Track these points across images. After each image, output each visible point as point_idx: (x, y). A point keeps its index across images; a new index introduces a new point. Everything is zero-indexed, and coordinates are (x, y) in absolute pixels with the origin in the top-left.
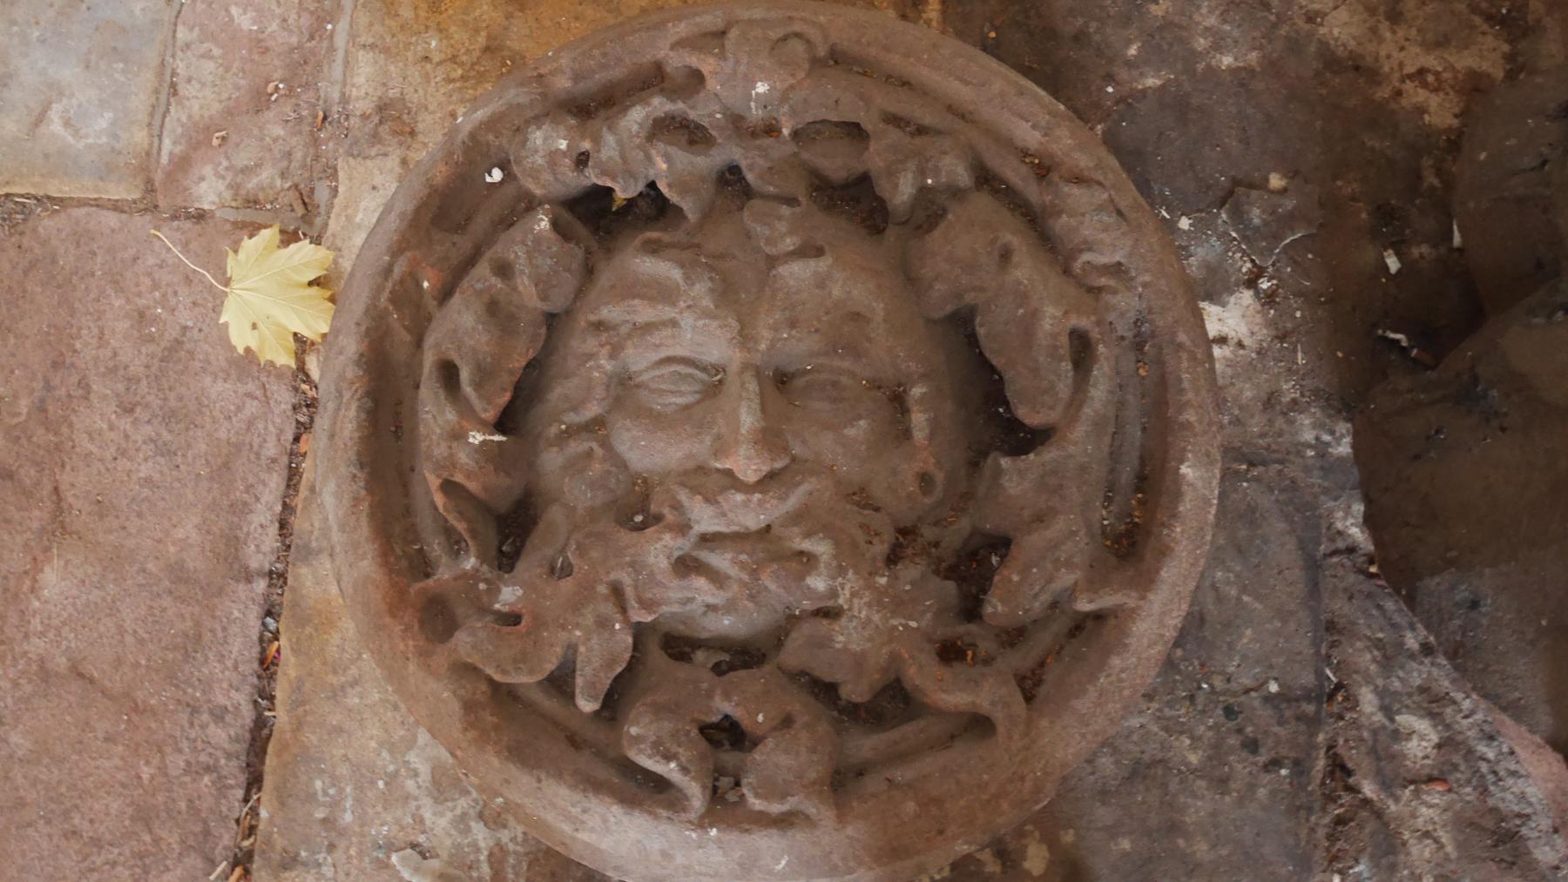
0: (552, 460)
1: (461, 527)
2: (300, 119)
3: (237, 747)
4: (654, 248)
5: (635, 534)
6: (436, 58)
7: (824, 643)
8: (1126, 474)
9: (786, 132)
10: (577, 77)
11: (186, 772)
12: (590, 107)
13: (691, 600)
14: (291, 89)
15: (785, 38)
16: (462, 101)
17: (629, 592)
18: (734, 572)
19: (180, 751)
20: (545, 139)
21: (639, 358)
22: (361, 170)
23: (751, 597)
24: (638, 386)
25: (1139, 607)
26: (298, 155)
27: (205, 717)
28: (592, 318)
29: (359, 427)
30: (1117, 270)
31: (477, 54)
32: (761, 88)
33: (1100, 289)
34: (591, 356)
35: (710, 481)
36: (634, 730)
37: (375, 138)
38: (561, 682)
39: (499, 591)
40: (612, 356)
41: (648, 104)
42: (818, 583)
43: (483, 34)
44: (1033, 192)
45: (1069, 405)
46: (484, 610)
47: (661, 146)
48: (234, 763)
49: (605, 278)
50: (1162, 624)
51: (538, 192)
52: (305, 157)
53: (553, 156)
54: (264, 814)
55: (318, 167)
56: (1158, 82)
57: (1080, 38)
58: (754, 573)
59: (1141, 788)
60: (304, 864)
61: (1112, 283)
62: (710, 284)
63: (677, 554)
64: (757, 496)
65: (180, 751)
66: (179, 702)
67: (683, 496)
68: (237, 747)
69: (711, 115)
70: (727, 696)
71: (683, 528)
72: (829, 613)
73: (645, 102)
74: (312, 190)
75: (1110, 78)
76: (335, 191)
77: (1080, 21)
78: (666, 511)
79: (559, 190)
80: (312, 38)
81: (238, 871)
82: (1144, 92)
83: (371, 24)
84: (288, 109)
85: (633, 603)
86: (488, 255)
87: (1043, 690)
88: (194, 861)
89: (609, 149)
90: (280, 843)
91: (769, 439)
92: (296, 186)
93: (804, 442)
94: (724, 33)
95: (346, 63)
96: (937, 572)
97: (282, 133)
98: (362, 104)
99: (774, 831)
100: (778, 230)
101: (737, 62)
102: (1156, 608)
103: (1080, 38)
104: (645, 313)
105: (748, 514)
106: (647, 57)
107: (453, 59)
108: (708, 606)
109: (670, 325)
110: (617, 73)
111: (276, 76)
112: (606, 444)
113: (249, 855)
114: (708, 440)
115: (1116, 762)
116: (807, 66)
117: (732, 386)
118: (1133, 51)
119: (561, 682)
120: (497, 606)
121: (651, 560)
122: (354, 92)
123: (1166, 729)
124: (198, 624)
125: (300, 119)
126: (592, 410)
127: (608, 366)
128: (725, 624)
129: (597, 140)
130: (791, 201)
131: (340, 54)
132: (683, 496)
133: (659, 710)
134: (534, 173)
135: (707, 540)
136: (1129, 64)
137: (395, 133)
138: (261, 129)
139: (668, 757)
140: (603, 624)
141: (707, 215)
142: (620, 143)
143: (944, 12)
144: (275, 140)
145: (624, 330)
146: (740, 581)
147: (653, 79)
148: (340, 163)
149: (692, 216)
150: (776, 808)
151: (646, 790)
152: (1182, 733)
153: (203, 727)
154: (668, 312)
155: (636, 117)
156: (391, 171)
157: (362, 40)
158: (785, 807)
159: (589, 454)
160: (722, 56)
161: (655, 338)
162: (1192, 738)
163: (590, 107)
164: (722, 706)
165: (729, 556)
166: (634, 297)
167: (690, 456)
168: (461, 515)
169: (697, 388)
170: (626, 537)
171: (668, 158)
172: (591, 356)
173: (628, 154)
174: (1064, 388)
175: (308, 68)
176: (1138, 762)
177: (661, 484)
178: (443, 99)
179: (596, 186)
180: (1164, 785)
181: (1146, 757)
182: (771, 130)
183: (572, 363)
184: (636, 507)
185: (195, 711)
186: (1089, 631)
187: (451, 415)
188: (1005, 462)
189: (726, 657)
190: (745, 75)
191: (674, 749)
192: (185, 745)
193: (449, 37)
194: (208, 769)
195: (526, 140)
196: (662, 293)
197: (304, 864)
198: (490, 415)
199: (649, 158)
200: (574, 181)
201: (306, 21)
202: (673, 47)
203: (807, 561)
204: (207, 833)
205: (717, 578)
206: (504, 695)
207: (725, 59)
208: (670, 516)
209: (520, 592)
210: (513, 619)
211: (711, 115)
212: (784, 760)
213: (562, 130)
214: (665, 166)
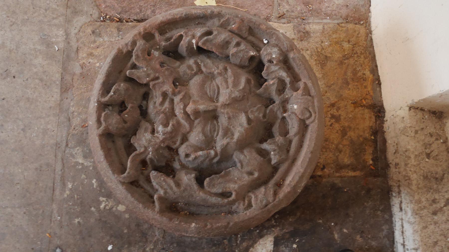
0: (191, 62)
1: (172, 40)
2: (303, 13)
3: (146, 16)
4: (248, 81)
5: (172, 82)
6: (323, 44)
7: (146, 131)
8: (193, 209)
9: (285, 115)
10: (293, 58)
11: (140, 6)
12: (285, 62)
13: (156, 97)
14: (310, 10)
15: (310, 112)
16: (311, 52)
17: (157, 82)
18: (164, 108)
19: (145, 4)
20: (275, 52)
21: (219, 80)
22: (290, 29)
23: (157, 112)
24: (212, 81)
25: (155, 212)
26: (293, 14)
27: (153, 9)
28: (228, 68)
29: (195, 14)
30: (250, 206)
31: (325, 54)
32: (295, 107)
33: (244, 201)
34: (218, 68)
35: (186, 99)
36: (122, 85)
37: (299, 32)
38: (134, 67)
39: (157, 51)
40: (218, 73)
41: (287, 77)
42: (160, 128)
43: (331, 55)
44: (273, 182)
45: (209, 192)
46: (152, 47)
47: (277, 82)
48: (143, 16)
49: (239, 71)
50: (153, 219)
51: (261, 52)
52: (293, 15)
53: (270, 54)
54: (130, 23)
55: (290, 19)
56: (336, 238)
57: (347, 215)
58: (163, 112)
59: (140, 235)
60: (118, 34)
61: (246, 204)
62: (238, 96)
63: (167, 93)
64: (183, 112)
65: (145, 4)
66: (156, 2)
67: (183, 93)
68: (146, 16)
69: (287, 94)
70: (132, 107)
71: (174, 94)
72: (153, 132)
73: (288, 76)
74: (284, 18)
75: (336, 224)
76: (285, 24)
77: (352, 215)
78: (178, 89)
79: (263, 57)
80: (325, 14)
81: (118, 20)
82: (333, 234)
83: (330, 28)
84: (305, 10)
85: (154, 82)
86: (242, 40)
87: (135, 188)
88: (120, 10)
89: (274, 68)
90: (124, 27)
91: (197, 113)
92: (285, 14)
93: (199, 123)
94: (310, 96)
95: (319, 23)
96: (167, 161)
97: (298, 9)
98: (307, 28)
99: (96, 119)
100: (256, 113)
101: (301, 99)
102: (156, 217)
103: (347, 215)
104: (230, 81)
105: (178, 111)
106: (301, 76)
107: (323, 49)
108: (156, 102)
109: (228, 86)
110: (297, 70)
111: (314, 7)
112: (196, 74)
113: (122, 22)
114: (198, 99)
115: (146, 229)
116: (302, 118)
117: (213, 104)
118: (345, 231)
119: (134, 67)
120: (153, 51)
121: (165, 86)
122: (311, 25)
123: (155, 242)
124: (174, 4)
125: (303, 13)
126: (204, 69)
127: (215, 73)
128: (151, 106)
129: (276, 65)
130: (264, 116)
131: (321, 21)
132: (183, 93)
133: (127, 90)
134: (266, 50)
135: (172, 101)
136: (341, 229)
137: (301, 36)
138: (299, 5)
139: (114, 92)
140: (148, 75)
141: (259, 96)
142: (276, 71)
143: (351, 177)
144: (296, 8)
145: (226, 76)
146: (161, 110)
147: (295, 78)
148: (291, 24)
149: (258, 91)
150: (102, 119)
151: (106, 87)
152: (154, 246)
153: (150, 8)
154: (230, 85)
155: (283, 74)
156: (291, 36)
157: (325, 26)
158: (102, 122)
159: (193, 70)
160: (302, 95)
161: (224, 84)
162: (153, 249)
163: (285, 62)
164: (129, 106)
165: (168, 106)
166: (234, 77)
167: (193, 95)
168: (175, 40)
169: (212, 96)
170: (171, 80)
171: (273, 84)
172: (218, 68)
173: (274, 73)
174: (214, 190)
175: (316, 14)
176: (147, 234)
177: (186, 88)
178: (311, 47)
179: (264, 66)
180: (140, 242)
181: (148, 237)
182: (285, 111)
183: (216, 64)
184: (179, 82)
185: (154, 6)
186: (148, 198)
187: (199, 34)
188: (193, 175)
189: (144, 108)
190: (298, 102)
191: (117, 94)
192: (146, 5)
193: (329, 47)
194: (141, 10)
195: (274, 47)
196: (236, 84)
197: (118, 34)
198: (200, 44)
199: (273, 79)
200: (265, 60)
201: (329, 12)
202: (305, 83)
203: (166, 125)
204: (126, 12)
205: (162, 104)
206: (129, 54)
207: (302, 96)
208: (177, 90)
209: (157, 56)
210: (149, 54)
211: (287, 94)
212: (114, 121)
213: (278, 56)
214: (271, 83)
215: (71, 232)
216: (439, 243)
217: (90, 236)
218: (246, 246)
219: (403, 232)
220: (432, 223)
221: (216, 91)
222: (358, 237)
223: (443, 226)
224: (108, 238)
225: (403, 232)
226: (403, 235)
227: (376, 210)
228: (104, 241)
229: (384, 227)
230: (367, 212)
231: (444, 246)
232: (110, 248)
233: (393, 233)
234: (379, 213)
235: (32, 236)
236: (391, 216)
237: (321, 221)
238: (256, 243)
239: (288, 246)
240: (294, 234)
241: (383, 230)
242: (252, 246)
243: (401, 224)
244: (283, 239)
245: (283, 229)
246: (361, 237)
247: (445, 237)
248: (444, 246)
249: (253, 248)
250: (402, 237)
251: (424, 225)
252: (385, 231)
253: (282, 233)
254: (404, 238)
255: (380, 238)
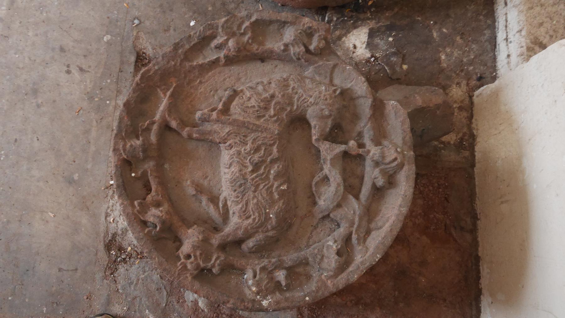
75: (435, 23)
103: (448, 16)
118: (444, 30)
136: (440, 29)
215: (151, 5)
216: (545, 25)
217: (171, 10)
218: (338, 34)
219: (506, 27)
220: (539, 4)
221: (266, 187)
222: (458, 38)
223: (549, 9)
224: (191, 14)
225: (506, 27)
226: (506, 29)
227: (478, 14)
228: (186, 16)
229: (485, 32)
230: (469, 15)
231: (549, 28)
232: (192, 23)
233: (495, 38)
234: (481, 17)
235: (108, 5)
236: (494, 21)
237: (419, 19)
238: (349, 33)
239: (383, 39)
240: (390, 28)
241: (485, 35)
242: (345, 35)
243: (504, 19)
244: (378, 31)
245: (379, 22)
246: (461, 38)
247: (551, 19)
248: (549, 28)
249: (346, 37)
250: (505, 32)
251: (530, 6)
252: (487, 35)
253: (378, 26)
254: (507, 33)
255: (481, 42)
